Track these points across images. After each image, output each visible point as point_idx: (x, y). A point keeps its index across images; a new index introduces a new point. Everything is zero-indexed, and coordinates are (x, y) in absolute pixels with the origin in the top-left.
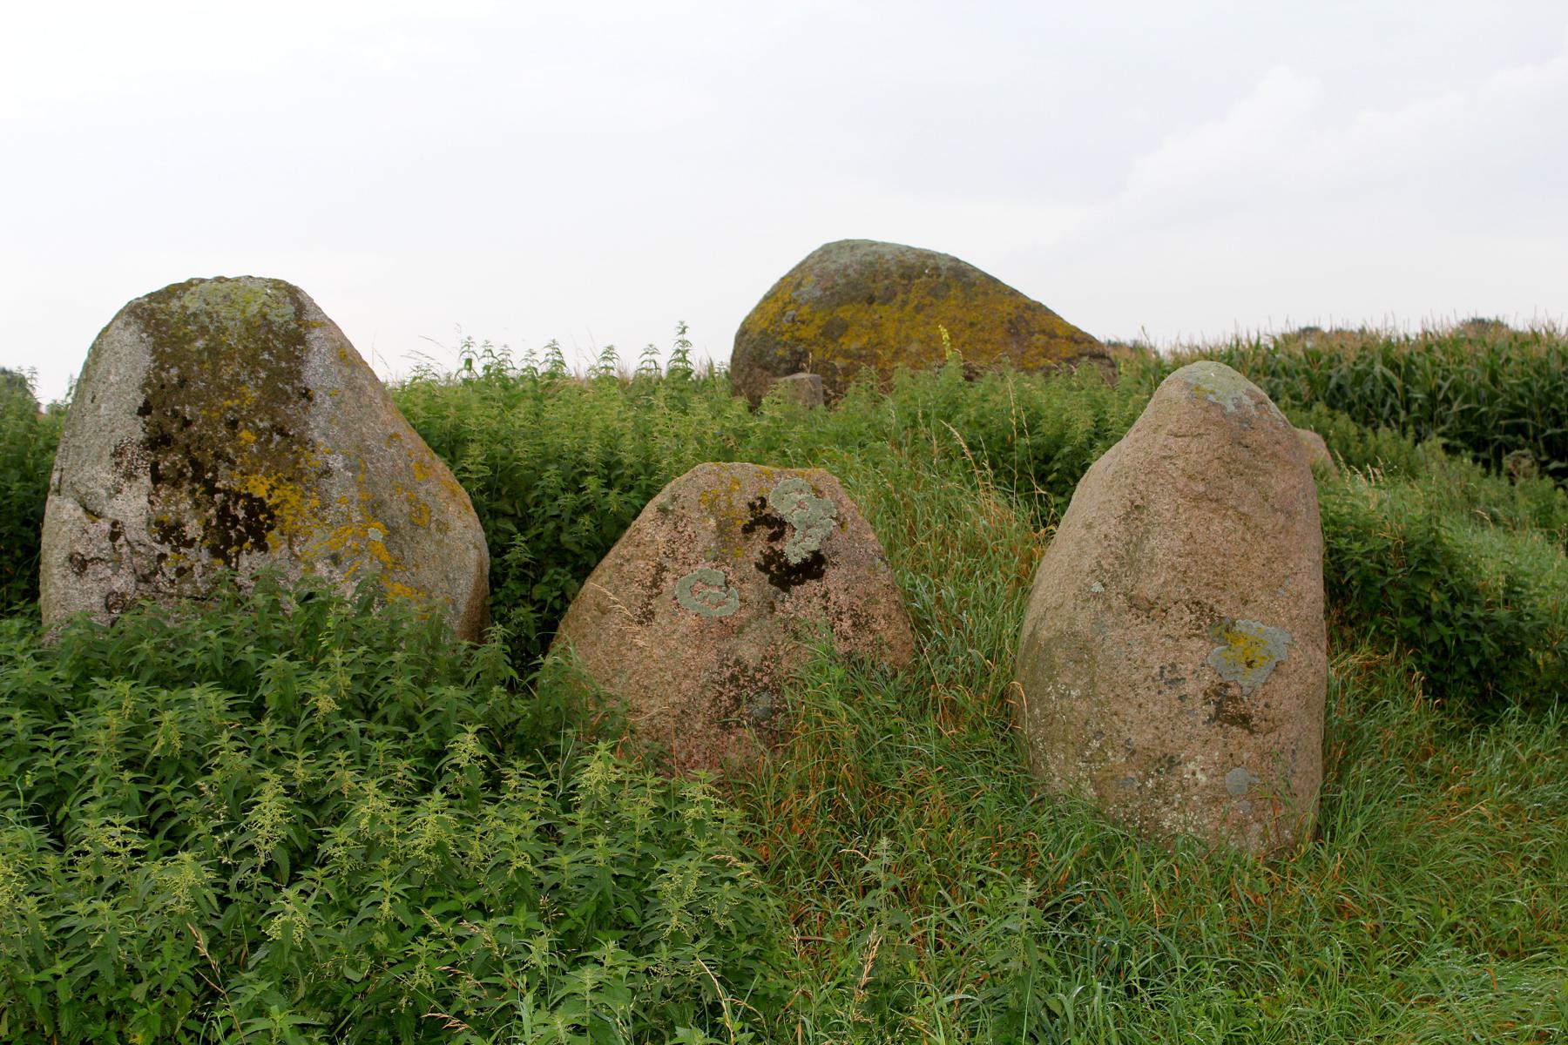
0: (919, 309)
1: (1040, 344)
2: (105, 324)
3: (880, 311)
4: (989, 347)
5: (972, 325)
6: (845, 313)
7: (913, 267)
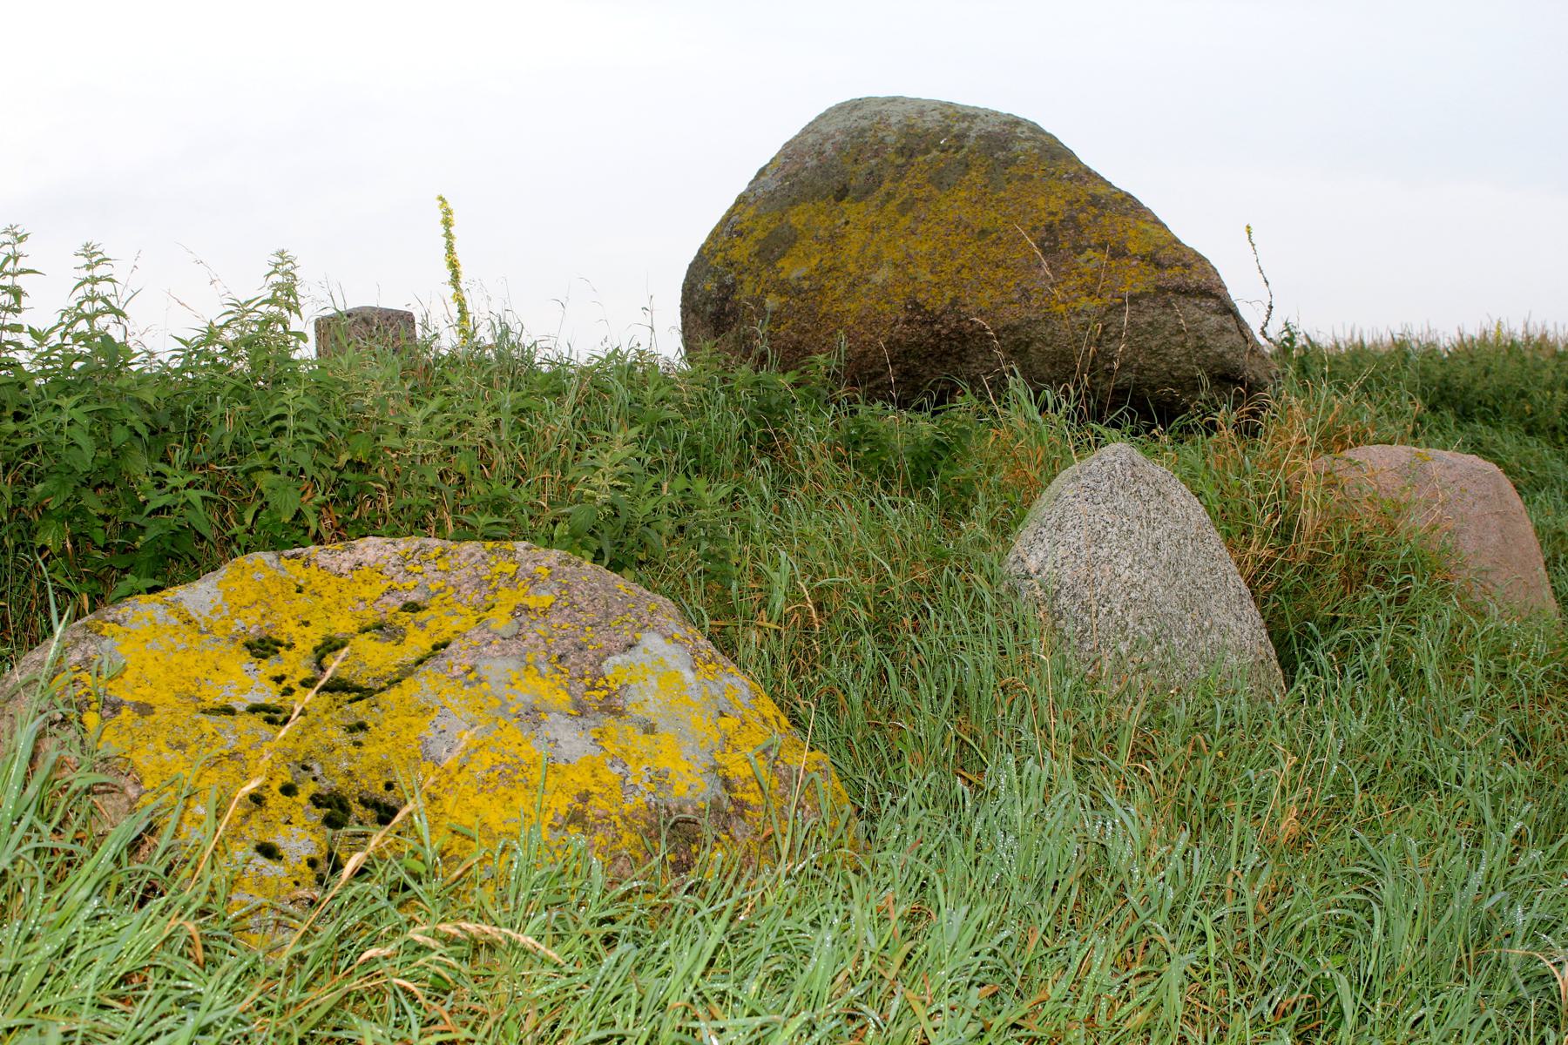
0: (904, 209)
1: (1088, 268)
4: (1000, 273)
5: (983, 232)
6: (797, 218)
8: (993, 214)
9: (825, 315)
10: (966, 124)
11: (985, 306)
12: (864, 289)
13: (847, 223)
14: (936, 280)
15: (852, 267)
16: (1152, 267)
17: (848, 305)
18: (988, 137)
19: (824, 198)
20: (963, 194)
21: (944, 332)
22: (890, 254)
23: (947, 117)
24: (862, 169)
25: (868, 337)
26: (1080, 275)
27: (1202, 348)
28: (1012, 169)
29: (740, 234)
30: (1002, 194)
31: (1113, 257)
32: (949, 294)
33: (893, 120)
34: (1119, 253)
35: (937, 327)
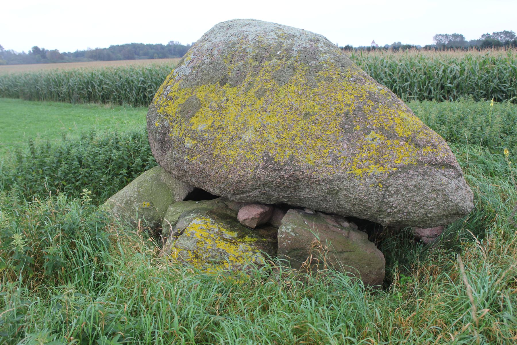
0: (260, 94)
1: (374, 145)
2: (240, 18)
3: (230, 92)
4: (319, 143)
5: (307, 115)
6: (201, 93)
7: (266, 49)
8: (312, 103)
9: (217, 156)
10: (290, 41)
11: (310, 164)
12: (238, 143)
13: (227, 100)
14: (280, 143)
15: (231, 128)
16: (413, 146)
17: (229, 152)
18: (304, 51)
19: (214, 83)
20: (293, 89)
21: (286, 176)
22: (253, 123)
23: (279, 36)
24: (234, 66)
25: (242, 173)
26: (369, 149)
27: (446, 201)
28: (320, 73)
29: (171, 99)
30: (316, 90)
31: (388, 138)
32: (289, 153)
33: (250, 38)
34: (391, 135)
35: (282, 173)
